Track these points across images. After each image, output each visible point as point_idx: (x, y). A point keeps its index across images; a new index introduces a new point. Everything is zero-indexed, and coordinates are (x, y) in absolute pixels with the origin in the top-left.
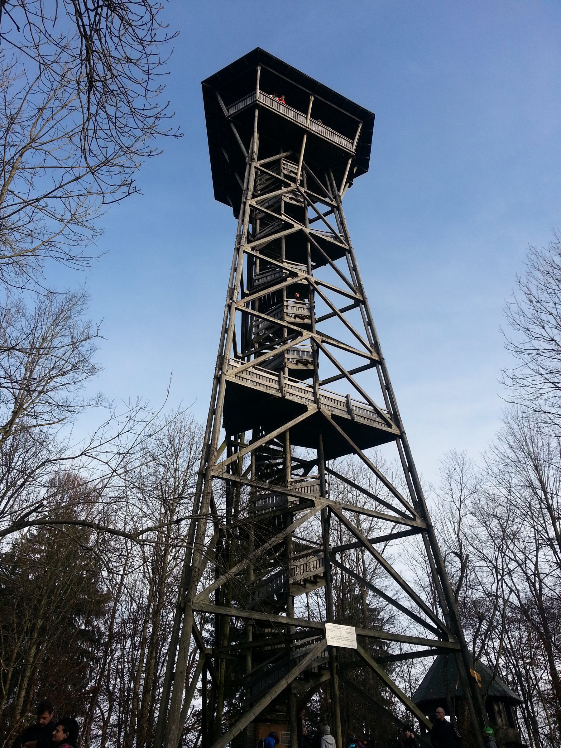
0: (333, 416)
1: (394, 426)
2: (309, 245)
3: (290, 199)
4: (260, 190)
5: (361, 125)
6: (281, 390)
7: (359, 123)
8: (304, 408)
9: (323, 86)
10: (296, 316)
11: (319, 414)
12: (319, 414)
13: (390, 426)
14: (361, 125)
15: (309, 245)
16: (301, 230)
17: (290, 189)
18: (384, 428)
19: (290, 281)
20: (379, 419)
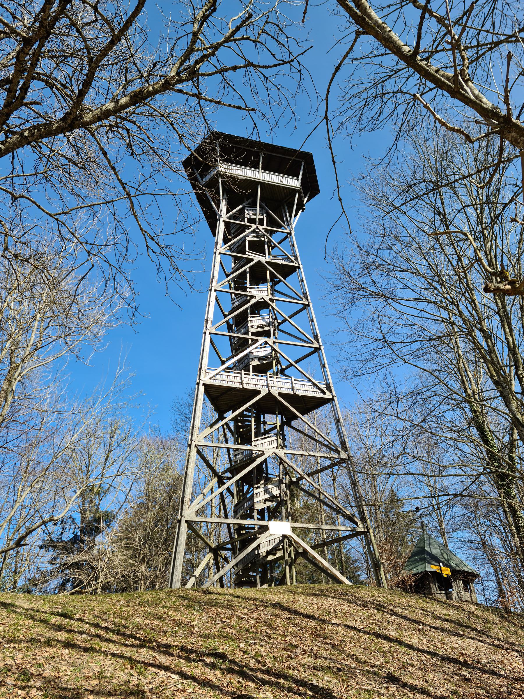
0: (280, 394)
1: (327, 392)
2: (268, 272)
3: (254, 237)
4: (234, 233)
5: (303, 164)
6: (293, 389)
7: (301, 162)
8: (258, 392)
9: (316, 181)
10: (258, 327)
11: (269, 394)
12: (269, 394)
13: (324, 393)
14: (303, 164)
15: (268, 272)
16: (259, 262)
17: (251, 229)
18: (321, 395)
19: (253, 301)
20: (315, 390)
